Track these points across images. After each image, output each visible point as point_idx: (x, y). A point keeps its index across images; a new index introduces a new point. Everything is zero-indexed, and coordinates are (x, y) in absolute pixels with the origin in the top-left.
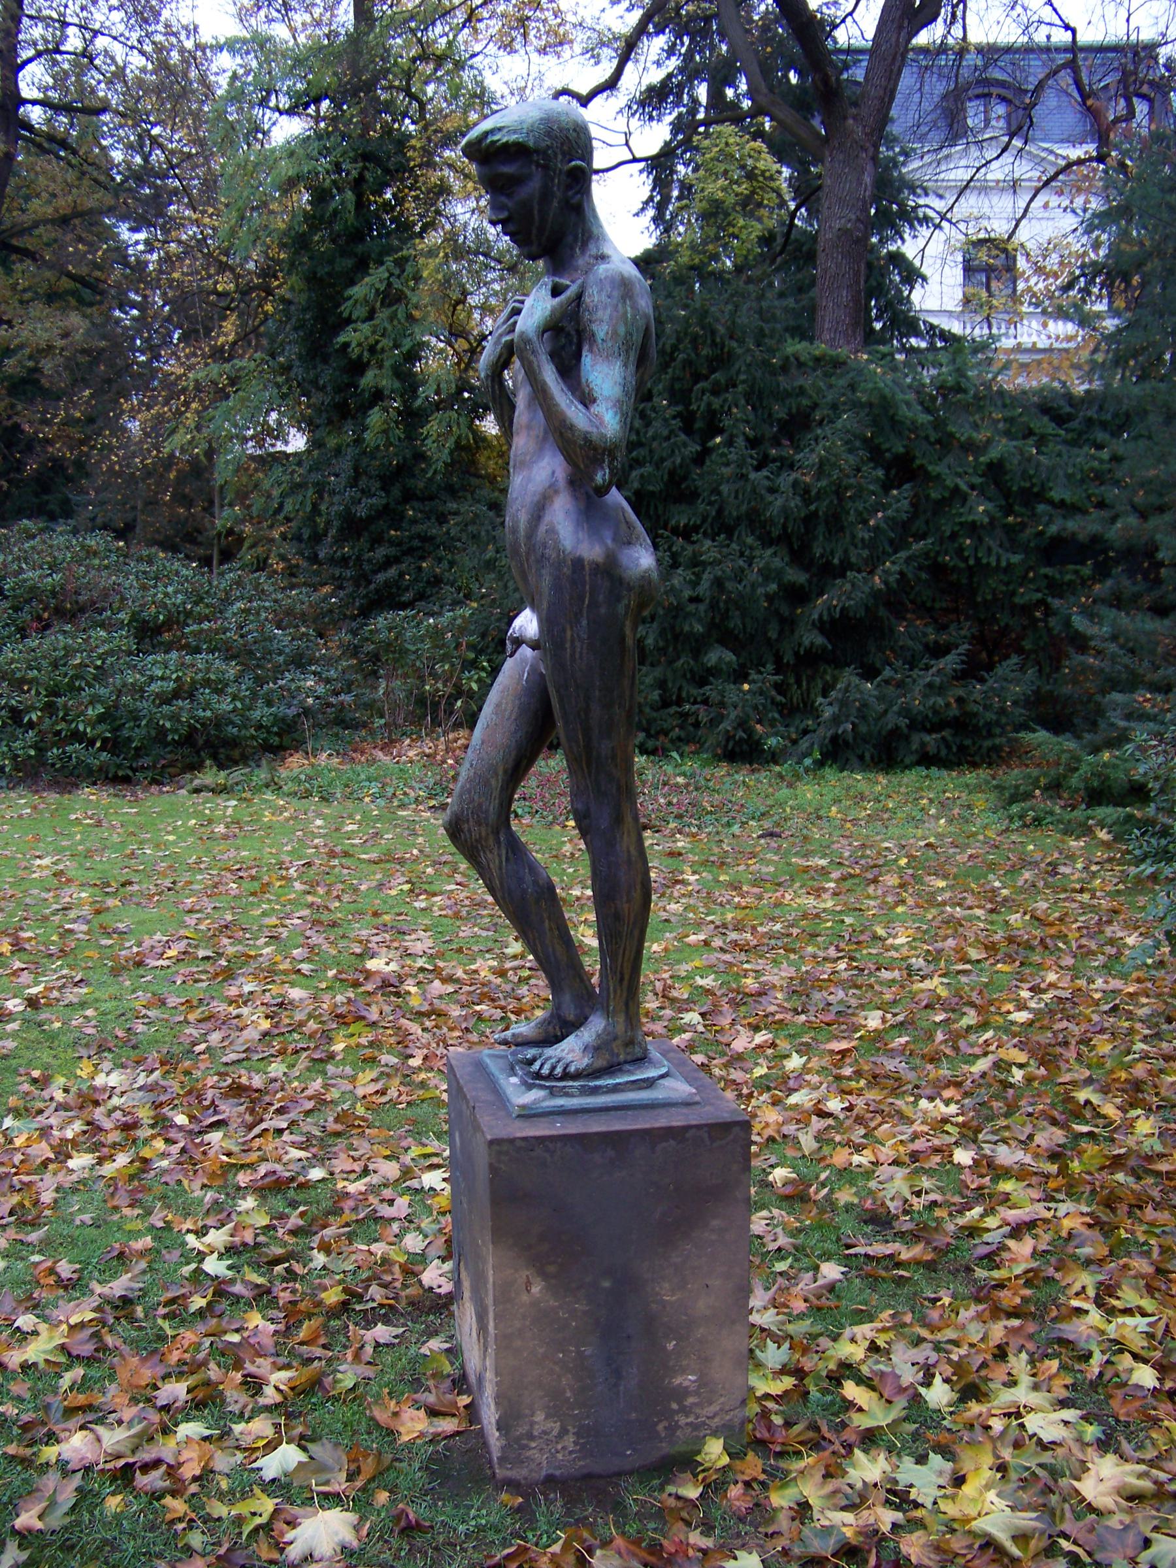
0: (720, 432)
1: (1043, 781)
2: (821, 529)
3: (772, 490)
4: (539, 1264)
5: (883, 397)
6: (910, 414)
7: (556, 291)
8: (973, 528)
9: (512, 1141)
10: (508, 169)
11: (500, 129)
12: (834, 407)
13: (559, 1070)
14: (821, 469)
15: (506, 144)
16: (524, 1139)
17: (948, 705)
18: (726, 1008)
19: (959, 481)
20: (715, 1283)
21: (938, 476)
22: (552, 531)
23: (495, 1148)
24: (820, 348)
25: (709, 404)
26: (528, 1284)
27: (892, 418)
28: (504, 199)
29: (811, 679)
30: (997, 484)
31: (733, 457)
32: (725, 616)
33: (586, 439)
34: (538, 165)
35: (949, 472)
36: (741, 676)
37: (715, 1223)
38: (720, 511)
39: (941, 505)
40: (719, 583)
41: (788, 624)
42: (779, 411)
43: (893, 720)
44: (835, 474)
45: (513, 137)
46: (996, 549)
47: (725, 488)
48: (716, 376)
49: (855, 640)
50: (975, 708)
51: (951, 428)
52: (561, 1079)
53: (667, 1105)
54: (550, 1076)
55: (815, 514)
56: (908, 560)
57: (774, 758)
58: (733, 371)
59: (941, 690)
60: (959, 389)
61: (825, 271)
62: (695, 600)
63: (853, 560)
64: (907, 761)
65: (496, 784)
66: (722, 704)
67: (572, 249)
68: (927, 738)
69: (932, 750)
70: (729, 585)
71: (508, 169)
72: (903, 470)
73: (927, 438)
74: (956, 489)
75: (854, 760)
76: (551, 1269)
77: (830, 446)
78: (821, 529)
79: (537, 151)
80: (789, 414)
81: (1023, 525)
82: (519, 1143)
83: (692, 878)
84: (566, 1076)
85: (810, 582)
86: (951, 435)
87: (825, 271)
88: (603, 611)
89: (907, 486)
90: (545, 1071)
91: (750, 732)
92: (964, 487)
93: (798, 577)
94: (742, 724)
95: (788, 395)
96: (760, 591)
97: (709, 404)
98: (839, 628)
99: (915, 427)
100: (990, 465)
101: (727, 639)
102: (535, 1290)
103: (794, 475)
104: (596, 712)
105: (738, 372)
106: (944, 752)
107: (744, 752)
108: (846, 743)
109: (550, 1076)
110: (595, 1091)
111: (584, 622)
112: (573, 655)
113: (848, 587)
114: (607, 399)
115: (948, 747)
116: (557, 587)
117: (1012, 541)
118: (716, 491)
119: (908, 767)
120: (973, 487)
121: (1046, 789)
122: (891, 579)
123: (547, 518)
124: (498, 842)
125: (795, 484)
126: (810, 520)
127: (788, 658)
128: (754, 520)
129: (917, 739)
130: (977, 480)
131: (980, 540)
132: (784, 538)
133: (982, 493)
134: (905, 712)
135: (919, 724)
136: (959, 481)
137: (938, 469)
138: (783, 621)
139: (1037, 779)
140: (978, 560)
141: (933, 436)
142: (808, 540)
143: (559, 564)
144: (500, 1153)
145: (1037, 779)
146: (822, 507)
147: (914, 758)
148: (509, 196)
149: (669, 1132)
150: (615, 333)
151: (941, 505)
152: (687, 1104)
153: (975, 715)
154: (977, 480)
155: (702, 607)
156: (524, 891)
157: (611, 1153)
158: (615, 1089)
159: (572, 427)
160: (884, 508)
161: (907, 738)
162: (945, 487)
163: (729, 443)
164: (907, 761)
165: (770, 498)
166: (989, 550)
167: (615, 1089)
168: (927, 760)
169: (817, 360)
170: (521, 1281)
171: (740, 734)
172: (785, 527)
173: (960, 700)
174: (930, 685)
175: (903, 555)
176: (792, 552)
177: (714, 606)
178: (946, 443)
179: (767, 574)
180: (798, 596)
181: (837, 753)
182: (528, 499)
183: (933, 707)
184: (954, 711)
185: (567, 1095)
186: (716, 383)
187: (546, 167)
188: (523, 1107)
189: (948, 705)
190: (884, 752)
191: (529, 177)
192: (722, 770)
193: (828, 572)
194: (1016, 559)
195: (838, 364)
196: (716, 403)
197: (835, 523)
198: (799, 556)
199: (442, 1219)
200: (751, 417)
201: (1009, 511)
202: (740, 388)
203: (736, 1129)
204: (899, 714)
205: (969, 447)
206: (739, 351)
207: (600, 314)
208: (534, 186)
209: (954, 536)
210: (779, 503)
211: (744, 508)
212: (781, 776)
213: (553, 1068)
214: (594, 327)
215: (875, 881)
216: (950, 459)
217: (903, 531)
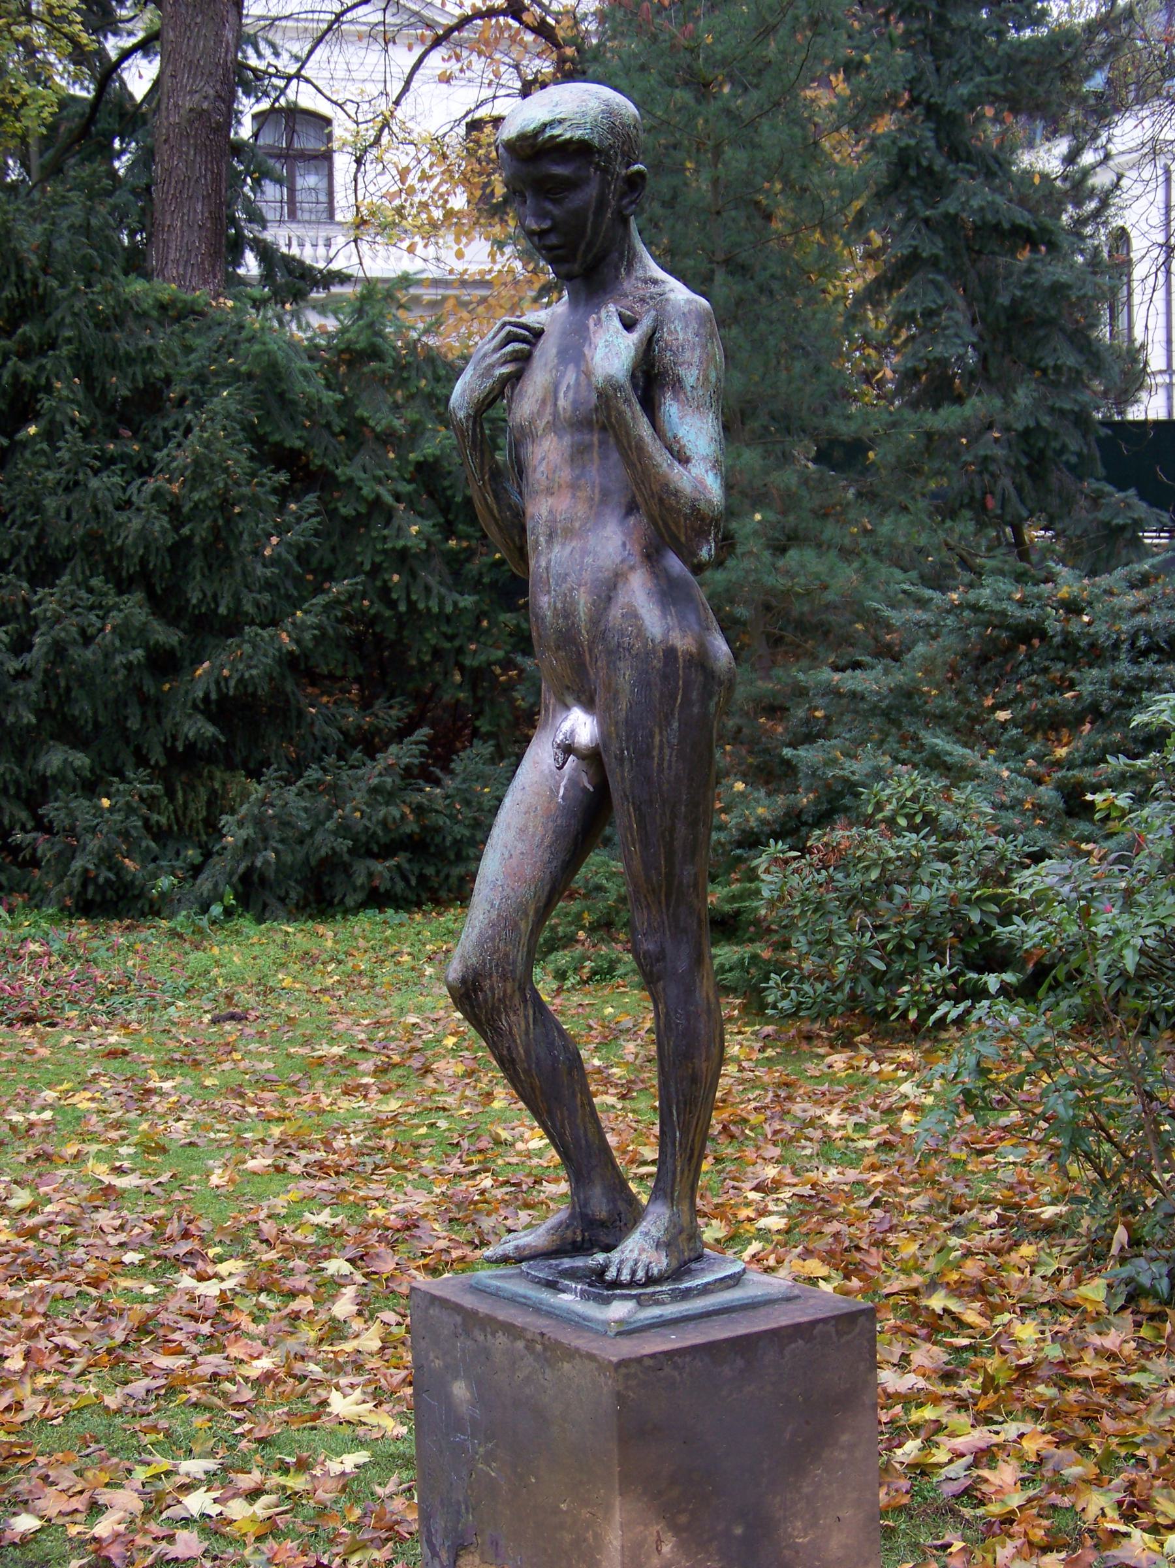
0: (36, 417)
1: (587, 919)
2: (197, 563)
3: (125, 505)
4: (669, 1513)
5: (273, 365)
6: (311, 390)
7: (629, 325)
8: (402, 557)
9: (639, 1360)
10: (559, 170)
11: (561, 121)
12: (201, 378)
13: (640, 1274)
14: (198, 474)
15: (569, 141)
16: (652, 1356)
17: (403, 816)
18: (382, 1248)
19: (380, 489)
20: (846, 1513)
21: (351, 481)
22: (632, 615)
23: (623, 1370)
24: (167, 290)
25: (16, 375)
26: (659, 1541)
27: (281, 396)
28: (549, 206)
29: (190, 787)
30: (431, 494)
31: (63, 454)
32: (66, 697)
33: (694, 508)
34: (597, 166)
35: (369, 476)
36: (91, 787)
37: (845, 1438)
38: (40, 538)
39: (352, 527)
40: (59, 650)
41: (154, 707)
42: (119, 385)
43: (326, 842)
44: (220, 481)
45: (578, 134)
46: (437, 589)
47: (50, 503)
48: (25, 329)
49: (250, 726)
50: (441, 821)
51: (361, 412)
52: (644, 1285)
53: (767, 1302)
54: (633, 1284)
55: (188, 540)
56: (328, 608)
57: (155, 909)
58: (50, 322)
59: (390, 797)
60: (375, 353)
61: (169, 172)
62: (23, 674)
63: (249, 608)
64: (350, 901)
65: (525, 927)
66: (71, 831)
67: (617, 269)
68: (379, 867)
69: (383, 885)
70: (74, 652)
71: (559, 170)
72: (302, 474)
73: (328, 426)
74: (377, 501)
75: (273, 902)
76: (683, 1519)
77: (208, 438)
78: (197, 563)
79: (599, 152)
80: (135, 390)
81: (470, 553)
82: (648, 1362)
83: (167, 1085)
84: (651, 1280)
85: (181, 643)
86: (363, 422)
87: (169, 172)
88: (696, 710)
89: (311, 497)
90: (625, 1277)
91: (118, 869)
92: (389, 499)
93: (166, 635)
94: (107, 858)
95: (130, 360)
96: (119, 659)
97: (16, 375)
98: (224, 708)
99: (314, 409)
100: (420, 466)
101: (71, 733)
102: (666, 1549)
103: (151, 485)
104: (682, 830)
105: (60, 324)
106: (400, 885)
107: (109, 900)
108: (263, 880)
109: (633, 1284)
110: (686, 1294)
111: (675, 725)
112: (660, 765)
113: (247, 648)
114: (704, 458)
115: (406, 879)
116: (643, 682)
117: (456, 574)
118: (36, 507)
119: (355, 910)
120: (398, 498)
121: (592, 929)
122: (307, 636)
123: (621, 598)
124: (525, 1001)
125: (157, 495)
126: (180, 549)
127: (157, 756)
128: (98, 552)
129: (361, 869)
130: (406, 488)
131: (414, 575)
132: (143, 579)
133: (411, 506)
134: (344, 829)
135: (373, 847)
136: (380, 489)
137: (349, 472)
138: (144, 700)
139: (579, 916)
140: (411, 604)
141: (338, 424)
142: (177, 579)
143: (648, 654)
144: (627, 1377)
145: (579, 916)
146: (200, 531)
147: (360, 897)
148: (554, 202)
149: (776, 1335)
150: (706, 379)
151: (352, 527)
152: (788, 1299)
153: (437, 830)
154: (406, 488)
155: (32, 686)
156: (555, 1059)
157: (740, 1363)
158: (705, 1290)
159: (676, 493)
160: (281, 530)
161: (347, 869)
162: (361, 498)
163: (51, 435)
164: (350, 901)
165: (121, 517)
166: (428, 589)
167: (705, 1290)
168: (377, 899)
169: (162, 307)
170: (652, 1539)
171: (105, 874)
172: (143, 562)
173: (420, 811)
174: (374, 790)
175: (321, 600)
176: (151, 596)
177: (49, 681)
178: (356, 434)
179: (123, 633)
180: (164, 663)
181: (255, 896)
182: (587, 576)
183: (384, 823)
184: (411, 826)
185: (658, 1303)
186: (26, 340)
187: (605, 171)
188: (620, 1322)
189: (403, 816)
190: (318, 890)
191: (586, 181)
192: (82, 930)
193: (211, 628)
194: (467, 601)
195: (192, 311)
196: (28, 372)
197: (219, 552)
198: (165, 603)
199: (264, 1547)
200: (81, 396)
201: (448, 530)
202: (65, 351)
203: (862, 1319)
204: (335, 833)
205: (387, 438)
206: (62, 293)
207: (688, 354)
208: (591, 192)
209: (376, 570)
210: (136, 523)
211: (80, 531)
212: (174, 933)
213: (634, 1273)
214: (681, 371)
215: (427, 1071)
216: (363, 458)
217: (311, 568)
